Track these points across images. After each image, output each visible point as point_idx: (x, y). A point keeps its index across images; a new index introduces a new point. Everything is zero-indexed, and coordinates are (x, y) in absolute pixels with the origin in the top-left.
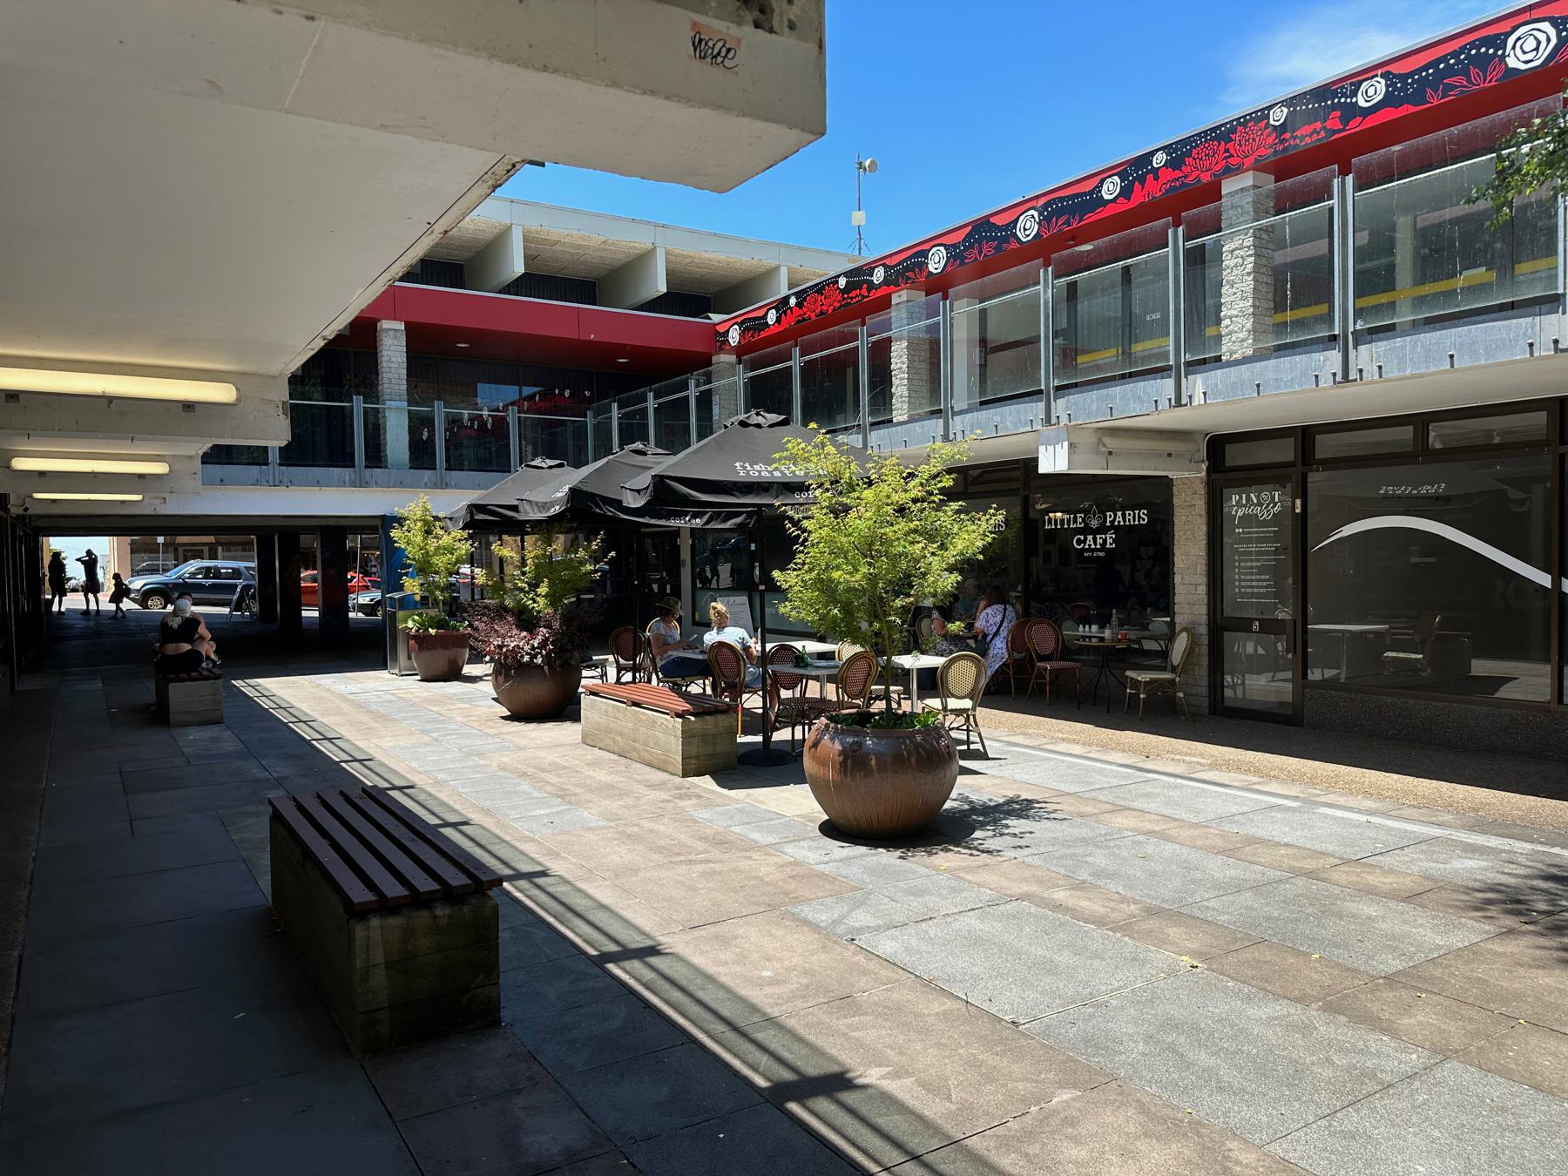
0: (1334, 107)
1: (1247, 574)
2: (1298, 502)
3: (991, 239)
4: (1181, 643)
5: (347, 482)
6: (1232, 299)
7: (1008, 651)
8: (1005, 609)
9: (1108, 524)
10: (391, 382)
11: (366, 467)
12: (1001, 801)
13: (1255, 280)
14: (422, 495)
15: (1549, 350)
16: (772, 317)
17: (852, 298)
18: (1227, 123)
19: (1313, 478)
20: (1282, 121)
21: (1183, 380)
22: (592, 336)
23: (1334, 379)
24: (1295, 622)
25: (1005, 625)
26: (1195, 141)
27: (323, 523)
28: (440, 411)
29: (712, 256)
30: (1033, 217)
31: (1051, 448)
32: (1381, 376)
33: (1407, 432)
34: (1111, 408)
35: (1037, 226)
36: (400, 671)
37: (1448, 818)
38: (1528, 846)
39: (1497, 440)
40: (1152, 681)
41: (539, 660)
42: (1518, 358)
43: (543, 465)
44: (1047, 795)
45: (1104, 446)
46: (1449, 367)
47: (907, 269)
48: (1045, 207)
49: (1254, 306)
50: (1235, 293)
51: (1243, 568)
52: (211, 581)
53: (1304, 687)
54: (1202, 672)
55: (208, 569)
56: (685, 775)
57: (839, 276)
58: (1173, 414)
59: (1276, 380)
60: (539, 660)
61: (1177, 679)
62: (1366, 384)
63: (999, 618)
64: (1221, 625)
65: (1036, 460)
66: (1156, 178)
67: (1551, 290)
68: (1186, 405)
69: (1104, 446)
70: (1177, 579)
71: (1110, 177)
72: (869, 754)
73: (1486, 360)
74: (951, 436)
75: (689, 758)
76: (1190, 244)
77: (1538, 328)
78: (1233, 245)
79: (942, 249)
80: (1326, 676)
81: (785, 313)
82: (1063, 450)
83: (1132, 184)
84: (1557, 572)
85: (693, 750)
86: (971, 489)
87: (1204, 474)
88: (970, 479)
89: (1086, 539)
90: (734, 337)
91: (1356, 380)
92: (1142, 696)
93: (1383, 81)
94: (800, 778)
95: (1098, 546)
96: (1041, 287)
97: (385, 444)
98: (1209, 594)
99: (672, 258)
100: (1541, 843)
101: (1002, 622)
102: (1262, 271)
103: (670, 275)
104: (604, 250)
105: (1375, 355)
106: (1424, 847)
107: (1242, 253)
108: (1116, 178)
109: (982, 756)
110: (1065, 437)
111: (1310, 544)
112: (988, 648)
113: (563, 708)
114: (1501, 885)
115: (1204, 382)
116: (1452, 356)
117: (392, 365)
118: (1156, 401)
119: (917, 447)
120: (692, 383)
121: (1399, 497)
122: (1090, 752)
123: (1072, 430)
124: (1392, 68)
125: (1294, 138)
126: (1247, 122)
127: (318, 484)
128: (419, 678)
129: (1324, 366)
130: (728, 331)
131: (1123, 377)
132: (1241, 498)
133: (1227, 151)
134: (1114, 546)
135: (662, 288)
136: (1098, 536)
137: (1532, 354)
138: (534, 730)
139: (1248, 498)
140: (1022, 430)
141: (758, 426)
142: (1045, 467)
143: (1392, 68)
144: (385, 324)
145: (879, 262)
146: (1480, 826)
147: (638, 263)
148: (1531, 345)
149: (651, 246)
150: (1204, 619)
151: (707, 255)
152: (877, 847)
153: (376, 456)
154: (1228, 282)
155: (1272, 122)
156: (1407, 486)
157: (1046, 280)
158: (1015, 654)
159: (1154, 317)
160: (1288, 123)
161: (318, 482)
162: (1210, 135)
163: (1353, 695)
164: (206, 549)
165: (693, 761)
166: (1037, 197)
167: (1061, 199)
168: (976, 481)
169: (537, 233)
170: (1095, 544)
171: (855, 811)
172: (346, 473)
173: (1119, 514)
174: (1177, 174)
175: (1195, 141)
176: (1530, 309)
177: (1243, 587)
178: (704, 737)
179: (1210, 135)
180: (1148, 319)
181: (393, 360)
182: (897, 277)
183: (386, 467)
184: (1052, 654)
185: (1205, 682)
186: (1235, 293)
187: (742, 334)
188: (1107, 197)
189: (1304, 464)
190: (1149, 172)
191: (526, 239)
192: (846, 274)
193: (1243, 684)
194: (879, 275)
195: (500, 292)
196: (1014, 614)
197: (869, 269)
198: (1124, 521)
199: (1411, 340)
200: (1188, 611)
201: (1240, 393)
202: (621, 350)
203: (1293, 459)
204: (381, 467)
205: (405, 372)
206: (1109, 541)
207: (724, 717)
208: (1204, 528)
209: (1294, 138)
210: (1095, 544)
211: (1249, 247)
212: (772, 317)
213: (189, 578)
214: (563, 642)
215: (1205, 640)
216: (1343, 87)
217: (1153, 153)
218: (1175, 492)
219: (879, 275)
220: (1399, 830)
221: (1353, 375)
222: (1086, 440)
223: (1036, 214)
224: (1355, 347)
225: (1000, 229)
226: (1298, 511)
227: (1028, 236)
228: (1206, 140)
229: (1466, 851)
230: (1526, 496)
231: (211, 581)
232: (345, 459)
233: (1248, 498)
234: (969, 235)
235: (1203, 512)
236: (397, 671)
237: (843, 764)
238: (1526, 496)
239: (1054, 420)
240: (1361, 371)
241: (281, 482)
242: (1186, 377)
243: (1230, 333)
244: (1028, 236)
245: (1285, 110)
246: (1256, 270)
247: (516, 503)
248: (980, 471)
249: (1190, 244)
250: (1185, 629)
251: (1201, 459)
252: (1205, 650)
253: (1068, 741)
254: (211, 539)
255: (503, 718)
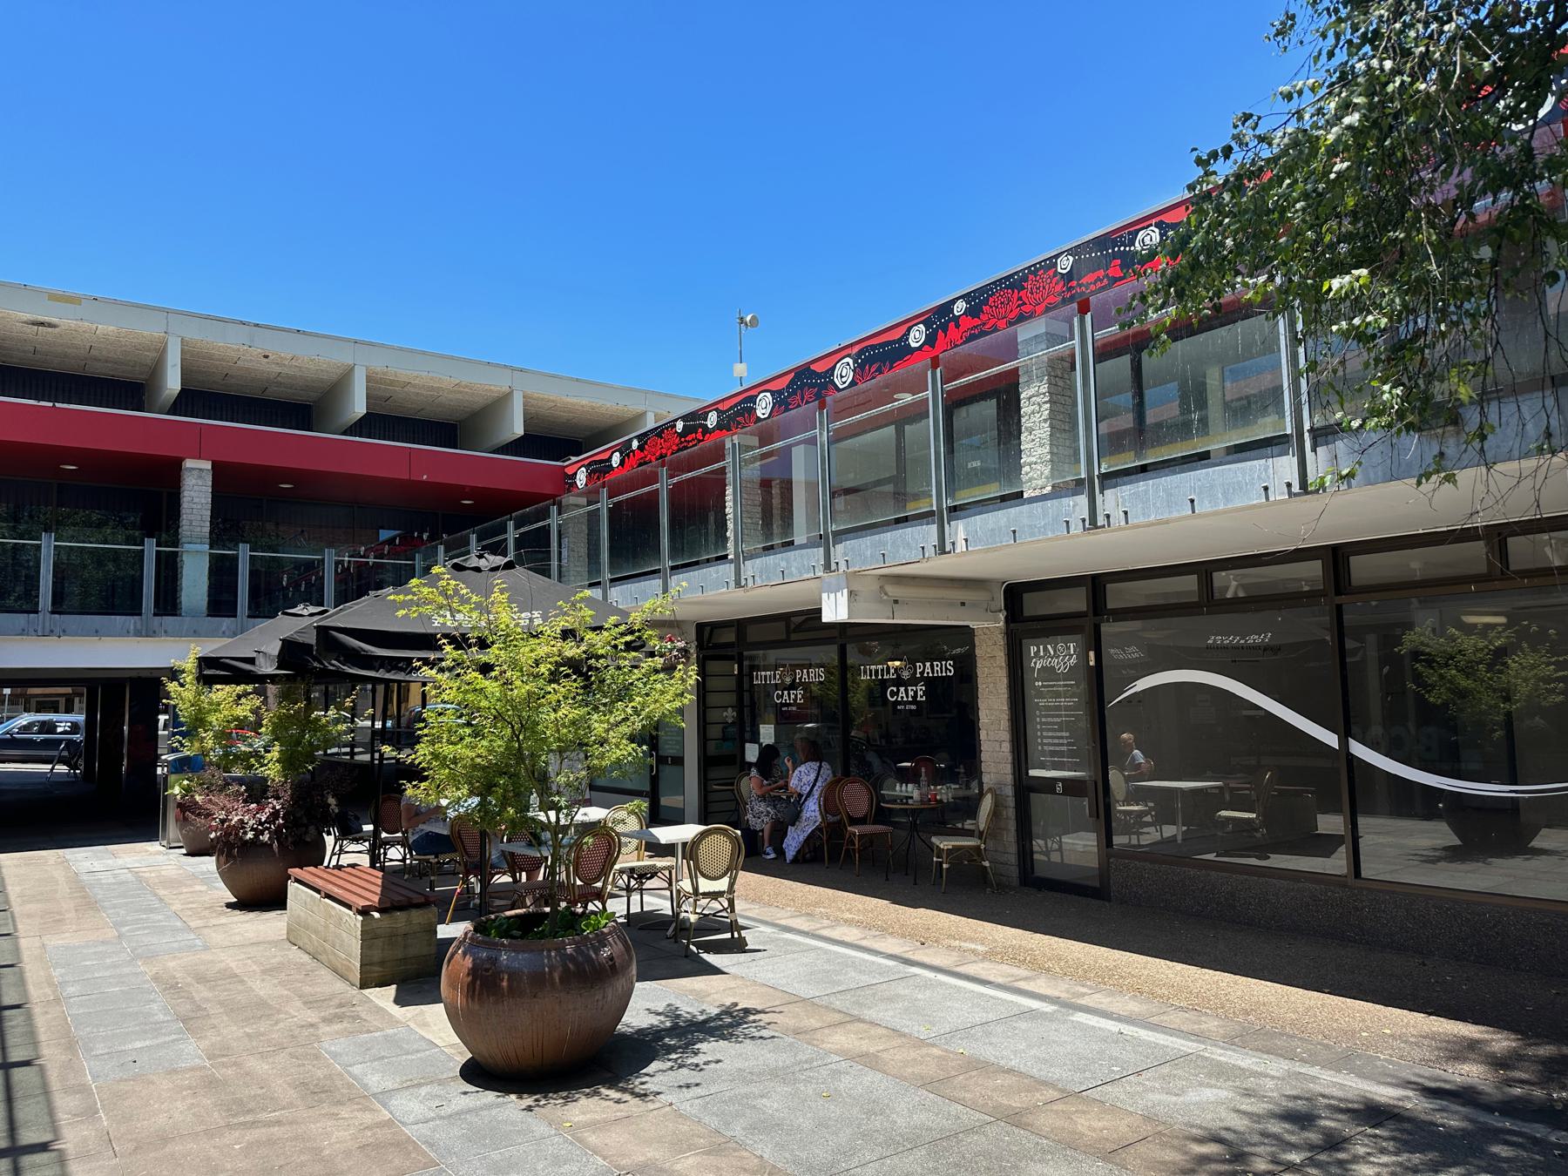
0: (1115, 256)
1: (1049, 730)
2: (1092, 654)
3: (812, 386)
4: (987, 804)
5: (132, 632)
6: (1030, 446)
7: (821, 813)
8: (820, 767)
9: (918, 675)
10: (191, 525)
11: (155, 615)
12: (715, 1011)
13: (1051, 426)
14: (193, 645)
15: (1283, 493)
16: (616, 460)
17: (689, 442)
18: (1020, 271)
19: (1106, 628)
20: (1068, 269)
21: (946, 526)
22: (425, 477)
23: (1084, 525)
24: (1096, 783)
25: (818, 784)
26: (992, 289)
27: (134, 674)
28: (244, 553)
29: (574, 400)
30: (848, 364)
31: (832, 596)
32: (1127, 523)
33: (1190, 583)
34: (883, 555)
35: (852, 373)
36: (169, 843)
37: (1211, 1025)
38: (1285, 1065)
39: (1306, 588)
40: (956, 848)
41: (265, 837)
42: (1255, 502)
43: (305, 612)
44: (777, 1003)
45: (886, 594)
46: (1190, 512)
47: (738, 414)
48: (861, 352)
49: (1051, 453)
50: (1033, 440)
51: (1045, 723)
52: (43, 736)
53: (1109, 856)
54: (1010, 837)
55: (43, 723)
56: (361, 988)
57: (676, 420)
58: (943, 561)
59: (1030, 526)
60: (265, 837)
61: (983, 846)
62: (1113, 531)
63: (812, 776)
64: (1025, 788)
65: (819, 611)
66: (957, 326)
67: (1279, 431)
68: (950, 552)
69: (886, 594)
70: (983, 735)
71: (916, 325)
72: (502, 972)
73: (1225, 505)
74: (743, 583)
75: (371, 964)
76: (949, 386)
77: (1271, 471)
78: (1032, 391)
79: (768, 394)
80: (1165, 835)
81: (628, 455)
82: (843, 598)
83: (935, 333)
84: (1343, 734)
85: (377, 955)
86: (794, 637)
87: (1002, 624)
88: (793, 626)
89: (898, 691)
90: (581, 479)
91: (1104, 526)
92: (945, 866)
93: (1157, 230)
94: (437, 1000)
95: (910, 699)
96: (817, 430)
97: (181, 590)
98: (1013, 752)
99: (188, 357)
100: (1303, 1060)
101: (816, 780)
102: (1058, 417)
103: (528, 421)
104: (461, 392)
105: (1120, 500)
106: (1166, 1069)
107: (1038, 399)
108: (921, 326)
109: (738, 946)
110: (844, 584)
111: (1107, 697)
112: (801, 811)
113: (271, 899)
114: (1227, 1129)
115: (966, 529)
116: (1192, 501)
117: (195, 506)
118: (923, 548)
119: (713, 592)
120: (511, 524)
121: (1225, 648)
122: (864, 938)
123: (852, 577)
124: (1164, 218)
125: (1080, 286)
126: (1037, 270)
127: (97, 633)
128: (184, 851)
129: (1074, 511)
130: (576, 473)
131: (898, 521)
132: (1039, 650)
133: (1020, 298)
134: (924, 699)
135: (519, 430)
136: (910, 688)
137: (1267, 498)
138: (251, 920)
139: (1045, 649)
140: (806, 576)
141: (478, 569)
142: (827, 617)
143: (1164, 218)
144: (189, 463)
145: (713, 406)
146: (1241, 1039)
147: (495, 407)
148: (1266, 489)
149: (508, 390)
150: (1009, 779)
151: (569, 400)
152: (508, 1092)
153: (168, 603)
154: (1026, 428)
155: (1059, 270)
156: (1235, 636)
157: (821, 423)
158: (829, 817)
159: (975, 465)
160: (1074, 271)
161: (97, 632)
162: (1005, 283)
163: (1157, 867)
164: (62, 701)
165: (376, 969)
166: (851, 345)
167: (873, 347)
168: (798, 628)
169: (384, 374)
170: (907, 697)
171: (509, 1043)
172: (131, 621)
173: (928, 664)
174: (977, 322)
175: (992, 289)
176: (1263, 451)
177: (1046, 744)
178: (392, 937)
179: (1005, 283)
180: (969, 466)
181: (196, 500)
182: (729, 422)
183: (180, 615)
184: (866, 816)
185: (1013, 849)
186: (1033, 440)
187: (589, 477)
188: (914, 345)
189: (1096, 614)
190: (950, 320)
191: (369, 379)
192: (684, 418)
193: (1060, 849)
194: (712, 420)
195: (344, 433)
196: (830, 772)
197: (701, 414)
198: (933, 673)
199: (1153, 485)
200: (994, 770)
201: (997, 539)
202: (464, 491)
203: (1085, 609)
204: (176, 615)
205: (209, 513)
206: (920, 693)
207: (420, 912)
208: (1005, 681)
209: (1080, 286)
210: (907, 697)
211: (1044, 394)
212: (616, 460)
213: (18, 733)
214: (298, 815)
215: (1011, 802)
216: (1121, 236)
217: (953, 302)
218: (977, 643)
219: (712, 420)
220: (1149, 1044)
221: (1101, 521)
222: (868, 588)
223: (851, 361)
224: (1102, 492)
225: (819, 375)
226: (1092, 663)
227: (844, 383)
228: (1001, 288)
229: (1209, 1075)
230: (1359, 645)
231: (43, 736)
232: (134, 609)
233: (1045, 649)
234: (792, 382)
235: (1004, 664)
236: (164, 843)
237: (471, 986)
238: (1359, 645)
239: (833, 567)
240: (1108, 516)
241: (52, 631)
242: (949, 523)
243: (1030, 480)
244: (844, 383)
245: (1071, 258)
246: (1052, 417)
247: (254, 655)
248: (804, 617)
249: (949, 386)
250: (990, 790)
251: (998, 608)
252: (1011, 812)
253: (849, 922)
254: (69, 690)
255: (229, 905)
